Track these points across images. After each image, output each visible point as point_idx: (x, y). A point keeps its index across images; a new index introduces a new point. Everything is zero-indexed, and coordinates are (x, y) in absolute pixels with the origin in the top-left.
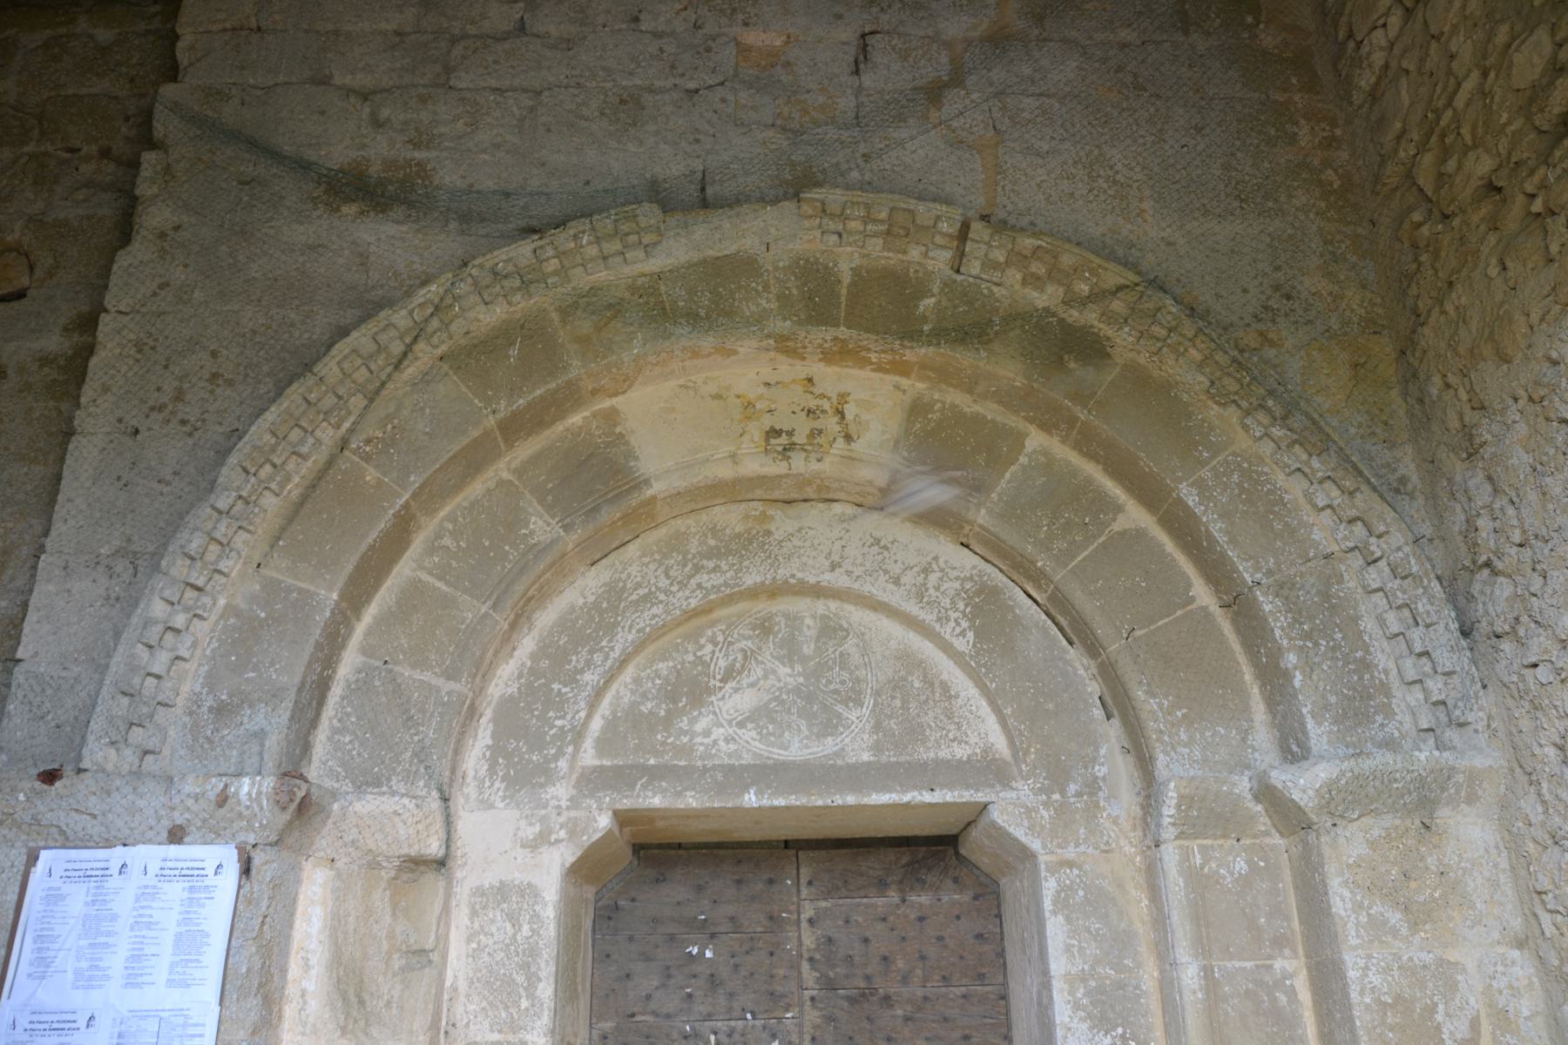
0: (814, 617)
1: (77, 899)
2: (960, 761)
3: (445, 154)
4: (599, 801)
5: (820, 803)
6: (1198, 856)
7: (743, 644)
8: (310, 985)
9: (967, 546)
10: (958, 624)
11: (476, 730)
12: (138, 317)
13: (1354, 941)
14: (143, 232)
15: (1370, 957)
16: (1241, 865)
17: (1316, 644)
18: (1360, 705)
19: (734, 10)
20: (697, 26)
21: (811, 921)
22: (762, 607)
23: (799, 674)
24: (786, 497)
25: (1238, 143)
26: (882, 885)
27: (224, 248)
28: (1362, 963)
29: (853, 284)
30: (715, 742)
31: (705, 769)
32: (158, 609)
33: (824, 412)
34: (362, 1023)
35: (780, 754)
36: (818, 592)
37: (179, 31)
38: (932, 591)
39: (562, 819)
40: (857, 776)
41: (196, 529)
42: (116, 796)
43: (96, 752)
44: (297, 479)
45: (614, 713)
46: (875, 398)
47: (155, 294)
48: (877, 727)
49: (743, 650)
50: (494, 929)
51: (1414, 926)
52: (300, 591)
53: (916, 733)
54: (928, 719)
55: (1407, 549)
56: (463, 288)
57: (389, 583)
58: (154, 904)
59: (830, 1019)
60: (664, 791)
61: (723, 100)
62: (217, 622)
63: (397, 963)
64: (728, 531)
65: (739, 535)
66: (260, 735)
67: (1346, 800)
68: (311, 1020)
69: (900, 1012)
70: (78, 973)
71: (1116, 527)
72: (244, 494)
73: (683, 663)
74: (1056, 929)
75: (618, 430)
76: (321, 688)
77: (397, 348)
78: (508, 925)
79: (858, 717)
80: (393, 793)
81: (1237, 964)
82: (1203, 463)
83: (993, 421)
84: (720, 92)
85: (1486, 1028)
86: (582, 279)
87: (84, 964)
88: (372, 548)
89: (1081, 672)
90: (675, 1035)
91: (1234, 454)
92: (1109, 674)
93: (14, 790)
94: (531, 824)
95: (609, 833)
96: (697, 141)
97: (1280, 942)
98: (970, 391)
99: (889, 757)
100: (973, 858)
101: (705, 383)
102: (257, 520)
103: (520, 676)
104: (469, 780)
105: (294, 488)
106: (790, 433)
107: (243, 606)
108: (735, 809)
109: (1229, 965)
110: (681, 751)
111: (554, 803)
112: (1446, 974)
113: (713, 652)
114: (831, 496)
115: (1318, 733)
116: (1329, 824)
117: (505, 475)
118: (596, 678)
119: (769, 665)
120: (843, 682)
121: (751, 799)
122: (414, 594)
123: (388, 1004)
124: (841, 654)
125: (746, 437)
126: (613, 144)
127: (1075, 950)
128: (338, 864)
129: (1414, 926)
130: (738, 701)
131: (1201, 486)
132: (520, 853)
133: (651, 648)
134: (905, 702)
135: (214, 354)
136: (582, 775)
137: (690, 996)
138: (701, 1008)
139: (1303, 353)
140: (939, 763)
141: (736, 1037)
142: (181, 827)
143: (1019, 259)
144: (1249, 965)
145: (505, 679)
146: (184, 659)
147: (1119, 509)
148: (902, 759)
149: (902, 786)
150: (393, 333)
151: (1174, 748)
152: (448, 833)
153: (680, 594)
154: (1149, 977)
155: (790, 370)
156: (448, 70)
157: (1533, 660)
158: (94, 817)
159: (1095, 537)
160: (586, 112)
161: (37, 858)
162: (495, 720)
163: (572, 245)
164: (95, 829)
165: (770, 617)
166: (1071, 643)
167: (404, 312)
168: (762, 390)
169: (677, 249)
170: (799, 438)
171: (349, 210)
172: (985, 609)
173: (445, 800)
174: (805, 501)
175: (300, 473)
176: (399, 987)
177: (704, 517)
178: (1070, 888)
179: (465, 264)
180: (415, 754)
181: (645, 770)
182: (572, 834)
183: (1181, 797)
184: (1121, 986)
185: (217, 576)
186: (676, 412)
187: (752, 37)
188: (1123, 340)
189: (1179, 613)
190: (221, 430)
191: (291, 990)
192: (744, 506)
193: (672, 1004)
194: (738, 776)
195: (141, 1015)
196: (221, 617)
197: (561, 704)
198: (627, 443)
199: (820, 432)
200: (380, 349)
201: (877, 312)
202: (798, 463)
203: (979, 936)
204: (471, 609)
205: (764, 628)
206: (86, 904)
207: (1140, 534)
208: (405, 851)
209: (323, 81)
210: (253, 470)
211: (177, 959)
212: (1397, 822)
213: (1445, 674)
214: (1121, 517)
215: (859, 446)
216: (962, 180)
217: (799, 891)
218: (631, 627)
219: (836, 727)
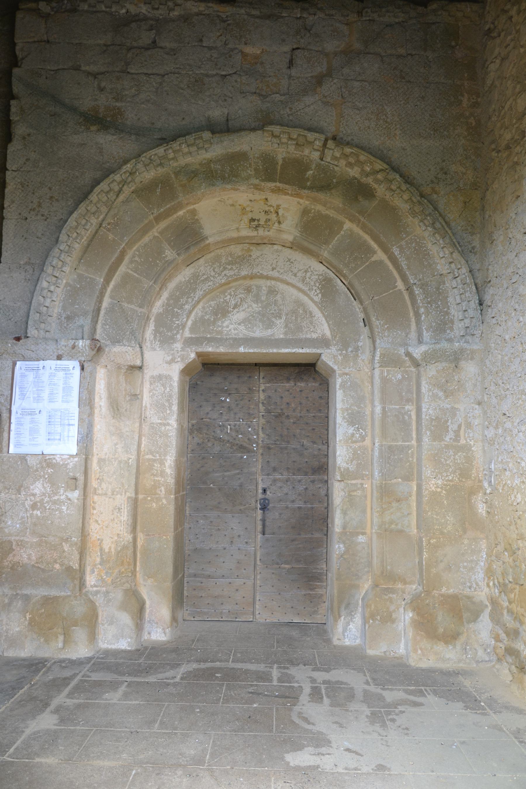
0: (266, 286)
1: (31, 376)
2: (314, 339)
3: (128, 104)
4: (191, 348)
5: (265, 351)
6: (386, 373)
7: (241, 296)
8: (102, 404)
9: (321, 263)
10: (316, 291)
11: (149, 324)
12: (20, 173)
13: (426, 400)
14: (17, 137)
15: (430, 405)
16: (399, 376)
17: (431, 306)
18: (442, 327)
19: (241, 36)
20: (226, 44)
21: (263, 391)
22: (248, 282)
23: (260, 307)
24: (257, 242)
25: (438, 104)
26: (288, 380)
27: (48, 144)
28: (427, 407)
29: (282, 165)
30: (230, 330)
31: (227, 339)
32: (45, 284)
33: (271, 212)
34: (119, 416)
35: (252, 334)
36: (267, 278)
37: (16, 41)
38: (308, 279)
39: (179, 355)
40: (278, 343)
41: (54, 257)
42: (40, 345)
43: (32, 332)
44: (85, 238)
45: (196, 319)
46: (290, 206)
47: (25, 163)
48: (286, 326)
49: (240, 298)
50: (158, 389)
51: (447, 397)
52: (90, 278)
53: (299, 329)
54: (304, 324)
55: (466, 274)
56: (140, 166)
57: (117, 273)
58: (55, 378)
59: (268, 422)
60: (213, 346)
61: (236, 81)
62: (63, 289)
63: (128, 398)
64: (236, 255)
65: (240, 257)
66: (82, 327)
67: (431, 357)
68: (103, 414)
69: (292, 421)
70: (34, 398)
71: (373, 259)
72: (69, 244)
73: (220, 302)
75: (196, 218)
76: (99, 310)
77: (117, 188)
78: (162, 388)
79: (280, 323)
80: (125, 346)
81: (393, 407)
82: (403, 239)
83: (333, 217)
84: (235, 77)
85: (463, 428)
86: (183, 161)
87: (36, 396)
88: (113, 263)
89: (358, 310)
90: (216, 426)
91: (415, 236)
92: (365, 310)
93: (7, 343)
94: (169, 356)
95: (195, 359)
96: (225, 100)
97: (408, 401)
98: (325, 206)
99: (290, 336)
100: (320, 371)
101: (228, 200)
102: (74, 253)
103: (163, 306)
104: (147, 341)
105: (84, 240)
106: (258, 220)
107: (71, 283)
108: (236, 353)
109: (391, 407)
110: (220, 332)
111: (176, 349)
112: (453, 411)
113: (230, 298)
114: (273, 242)
115: (426, 335)
116: (425, 365)
117: (156, 234)
118: (189, 307)
119: (249, 303)
120: (275, 310)
121: (242, 350)
122: (126, 278)
123: (126, 410)
124: (275, 301)
125: (242, 222)
126: (193, 101)
127: (345, 401)
128: (109, 367)
129: (447, 397)
130: (238, 316)
131: (401, 248)
132: (165, 365)
133: (208, 296)
134: (296, 318)
135: (50, 189)
136: (185, 340)
137: (221, 413)
138: (225, 417)
139: (447, 197)
140: (307, 339)
141: (237, 427)
142: (61, 355)
143: (345, 156)
144: (397, 407)
145: (158, 307)
146: (54, 301)
147: (375, 252)
148: (294, 337)
149: (292, 346)
150: (115, 183)
151: (382, 338)
152: (142, 358)
153: (219, 278)
155: (259, 196)
156: (127, 64)
157: (493, 316)
158: (33, 351)
159: (365, 263)
160: (182, 86)
161: (16, 364)
163: (179, 148)
164: (33, 355)
165: (250, 286)
166: (355, 299)
167: (118, 175)
168: (249, 203)
170: (262, 222)
171: (94, 128)
173: (141, 347)
174: (264, 244)
175: (86, 236)
176: (129, 405)
177: (227, 249)
178: (346, 382)
179: (140, 156)
180: (131, 333)
181: (206, 339)
182: (182, 360)
183: (381, 354)
184: (359, 412)
185: (62, 273)
186: (216, 210)
187: (249, 50)
188: (381, 190)
189: (391, 291)
190: (56, 218)
191: (96, 405)
192: (242, 245)
193: (215, 416)
194: (238, 342)
195: (56, 410)
196: (65, 287)
197: (177, 316)
198: (199, 223)
199: (269, 220)
200: (111, 190)
201: (291, 175)
203: (321, 397)
204: (146, 284)
206: (34, 378)
207: (381, 262)
208: (129, 364)
209: (77, 68)
210: (71, 235)
211: (64, 394)
212: (447, 365)
213: (471, 318)
214: (375, 256)
215: (283, 226)
216: (327, 120)
217: (259, 381)
218: (201, 289)
219: (272, 326)
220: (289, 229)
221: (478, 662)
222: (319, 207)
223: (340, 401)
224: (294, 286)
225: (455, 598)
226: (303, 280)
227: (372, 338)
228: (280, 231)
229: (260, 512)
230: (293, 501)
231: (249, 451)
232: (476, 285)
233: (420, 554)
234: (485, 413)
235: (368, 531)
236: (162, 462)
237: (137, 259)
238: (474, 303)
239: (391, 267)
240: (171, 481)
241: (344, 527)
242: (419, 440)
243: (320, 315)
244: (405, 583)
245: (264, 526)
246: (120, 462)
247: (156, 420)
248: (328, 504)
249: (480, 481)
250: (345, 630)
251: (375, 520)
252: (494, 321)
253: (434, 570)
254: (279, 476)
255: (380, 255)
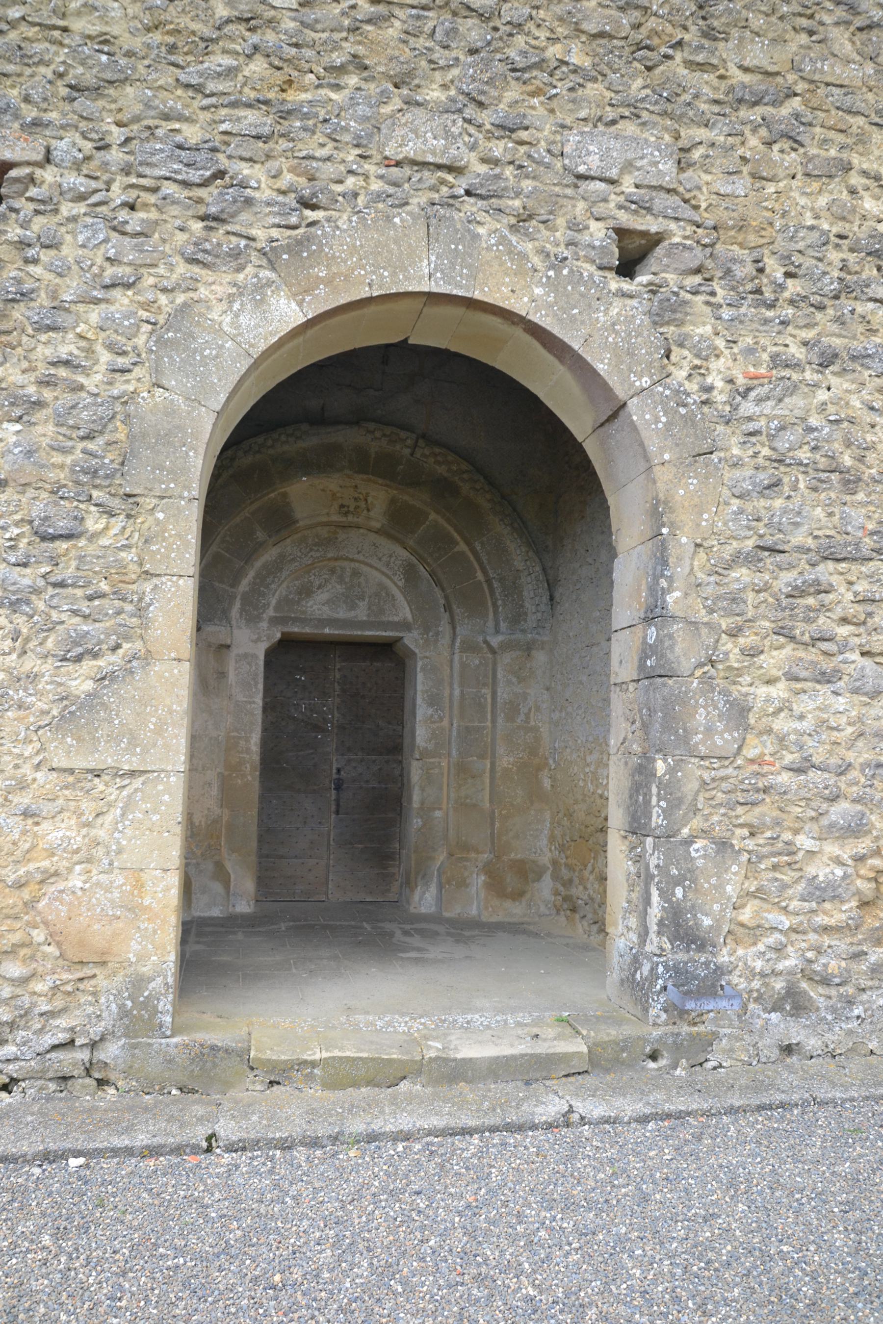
16: (477, 662)
18: (517, 619)
22: (332, 564)
35: (335, 615)
36: (352, 560)
40: (362, 625)
46: (379, 496)
48: (369, 608)
51: (519, 683)
67: (507, 646)
74: (420, 677)
92: (446, 598)
97: (485, 685)
99: (372, 619)
110: (304, 612)
112: (525, 696)
115: (503, 626)
121: (327, 631)
129: (519, 683)
130: (322, 596)
131: (482, 543)
140: (389, 622)
145: (244, 585)
154: (446, 693)
162: (242, 599)
169: (313, 440)
170: (351, 509)
172: (410, 573)
181: (291, 618)
182: (268, 639)
188: (465, 488)
194: (323, 622)
201: (382, 468)
202: (350, 518)
205: (333, 571)
207: (462, 553)
215: (372, 514)
220: (378, 516)
221: (540, 916)
222: (406, 498)
223: (421, 684)
224: (376, 569)
225: (522, 861)
226: (388, 564)
227: (453, 623)
228: (369, 518)
229: (333, 792)
230: (367, 781)
231: (323, 730)
232: (548, 581)
233: (492, 825)
234: (552, 698)
235: (444, 806)
236: (247, 740)
237: (228, 538)
238: (545, 599)
239: (472, 558)
240: (256, 758)
241: (422, 803)
242: (494, 721)
243: (402, 599)
244: (477, 852)
245: (338, 805)
246: (211, 739)
247: (241, 698)
248: (403, 784)
249: (546, 759)
250: (421, 899)
251: (452, 795)
252: (561, 617)
253: (504, 838)
254: (353, 757)
255: (462, 547)
